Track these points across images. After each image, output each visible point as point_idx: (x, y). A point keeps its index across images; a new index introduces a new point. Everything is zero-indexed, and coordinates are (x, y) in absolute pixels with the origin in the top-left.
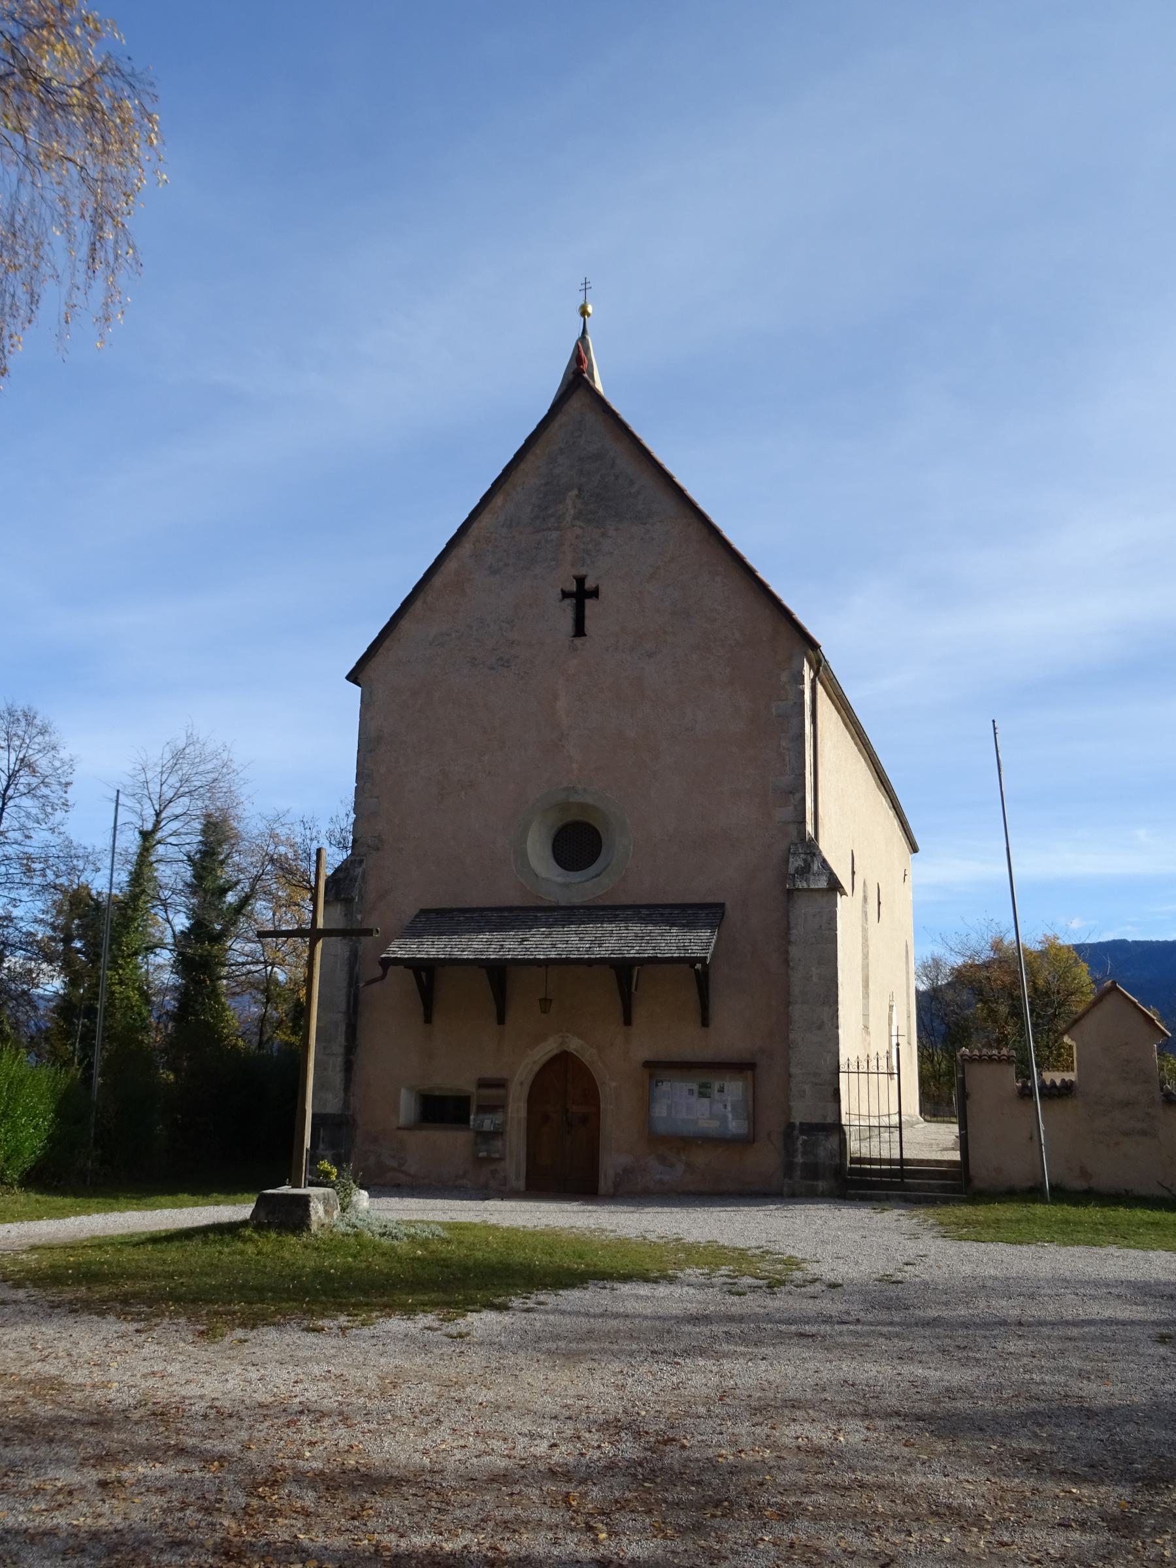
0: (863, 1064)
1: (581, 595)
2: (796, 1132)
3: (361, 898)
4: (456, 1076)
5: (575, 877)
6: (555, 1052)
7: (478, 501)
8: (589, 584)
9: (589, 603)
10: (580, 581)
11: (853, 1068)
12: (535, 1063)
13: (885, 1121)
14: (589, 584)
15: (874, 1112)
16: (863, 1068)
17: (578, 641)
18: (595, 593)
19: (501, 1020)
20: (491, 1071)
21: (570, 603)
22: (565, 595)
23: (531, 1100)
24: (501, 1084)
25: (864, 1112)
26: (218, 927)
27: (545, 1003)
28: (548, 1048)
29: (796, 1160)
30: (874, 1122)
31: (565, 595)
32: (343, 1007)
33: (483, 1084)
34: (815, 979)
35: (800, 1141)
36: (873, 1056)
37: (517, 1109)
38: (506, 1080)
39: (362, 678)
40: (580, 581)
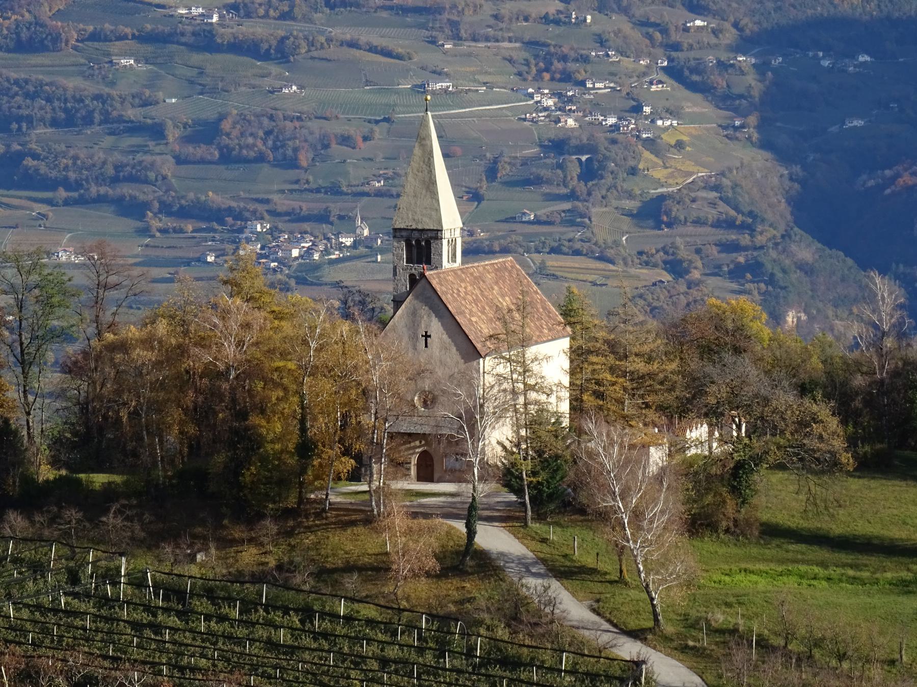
10: (426, 332)
18: (430, 336)
40: (426, 332)
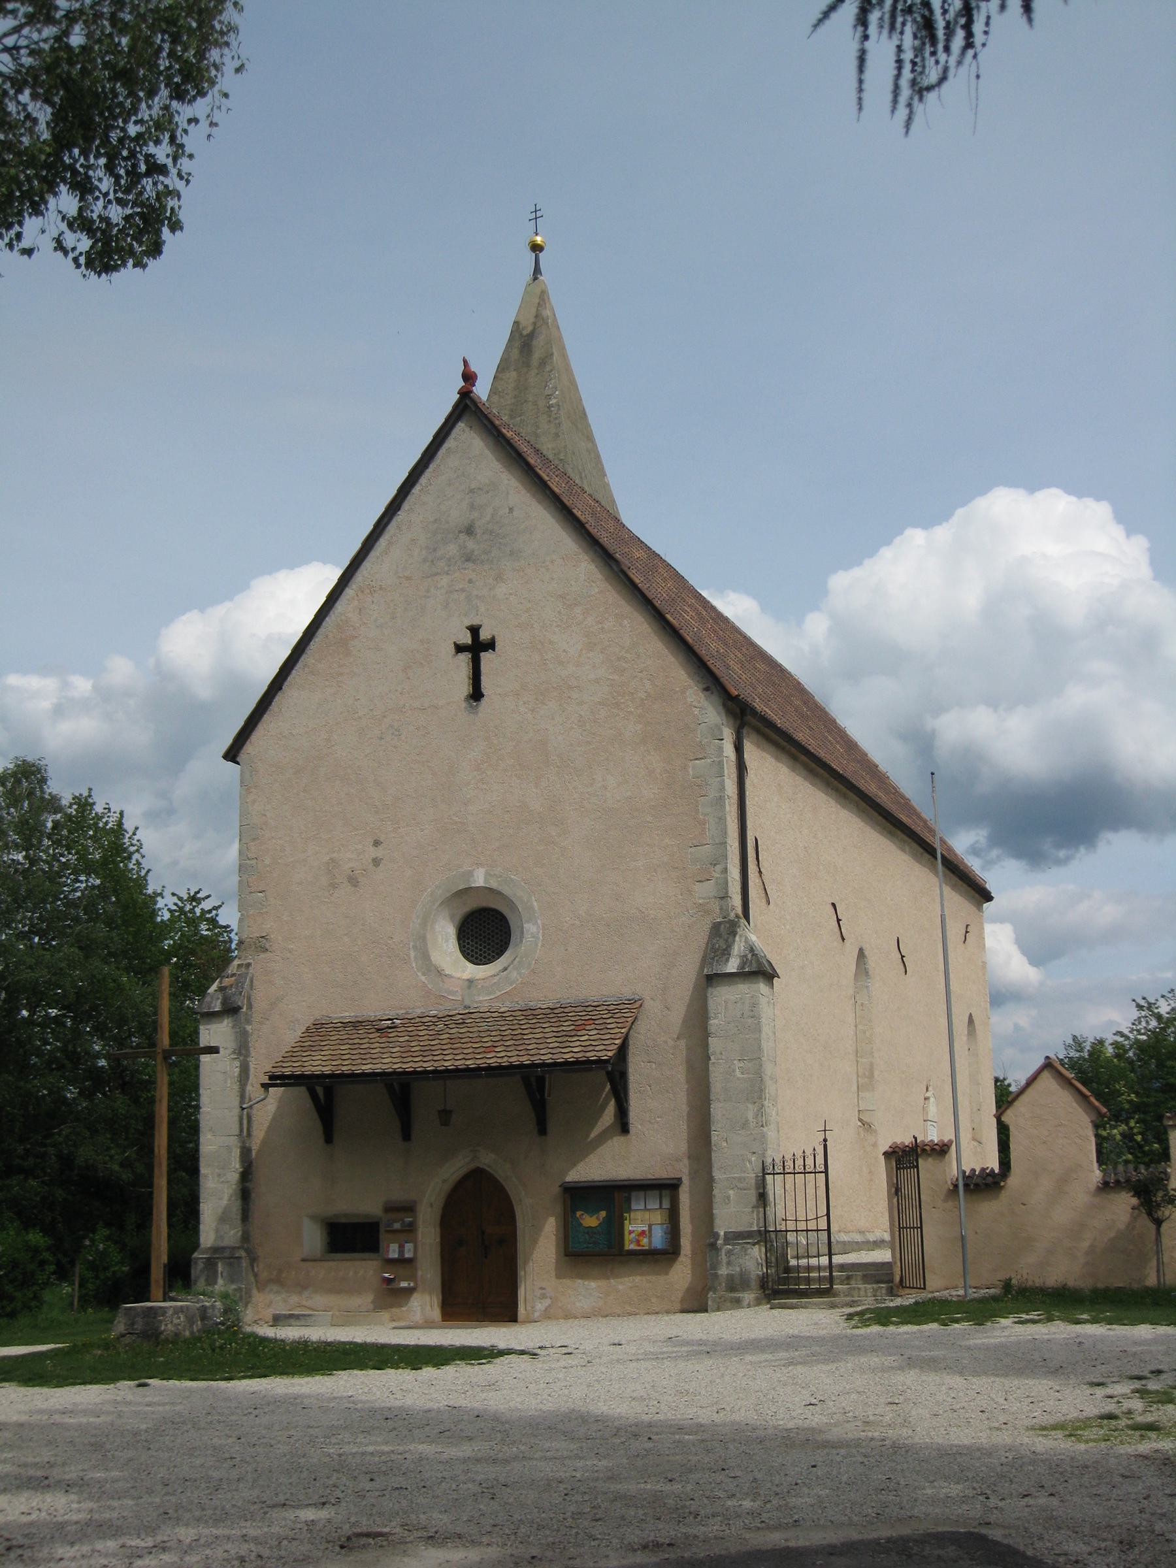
0: (789, 1164)
1: (477, 647)
2: (720, 1242)
3: (250, 1007)
4: (362, 1201)
5: (480, 972)
6: (465, 1170)
7: (360, 545)
8: (484, 635)
9: (485, 657)
10: (474, 630)
11: (779, 1169)
12: (444, 1181)
13: (812, 1225)
14: (484, 635)
15: (802, 1217)
16: (779, 1169)
17: (473, 710)
18: (491, 645)
19: (407, 1135)
20: (397, 1194)
21: (465, 658)
22: (459, 649)
23: (445, 1223)
24: (409, 1208)
25: (811, 1216)
26: (97, 1048)
27: (445, 1116)
28: (454, 1169)
29: (720, 1272)
30: (801, 1226)
31: (459, 649)
32: (235, 1129)
33: (390, 1208)
34: (738, 1074)
35: (723, 1252)
36: (809, 1152)
37: (428, 1235)
38: (415, 1202)
39: (242, 757)
40: (474, 630)
